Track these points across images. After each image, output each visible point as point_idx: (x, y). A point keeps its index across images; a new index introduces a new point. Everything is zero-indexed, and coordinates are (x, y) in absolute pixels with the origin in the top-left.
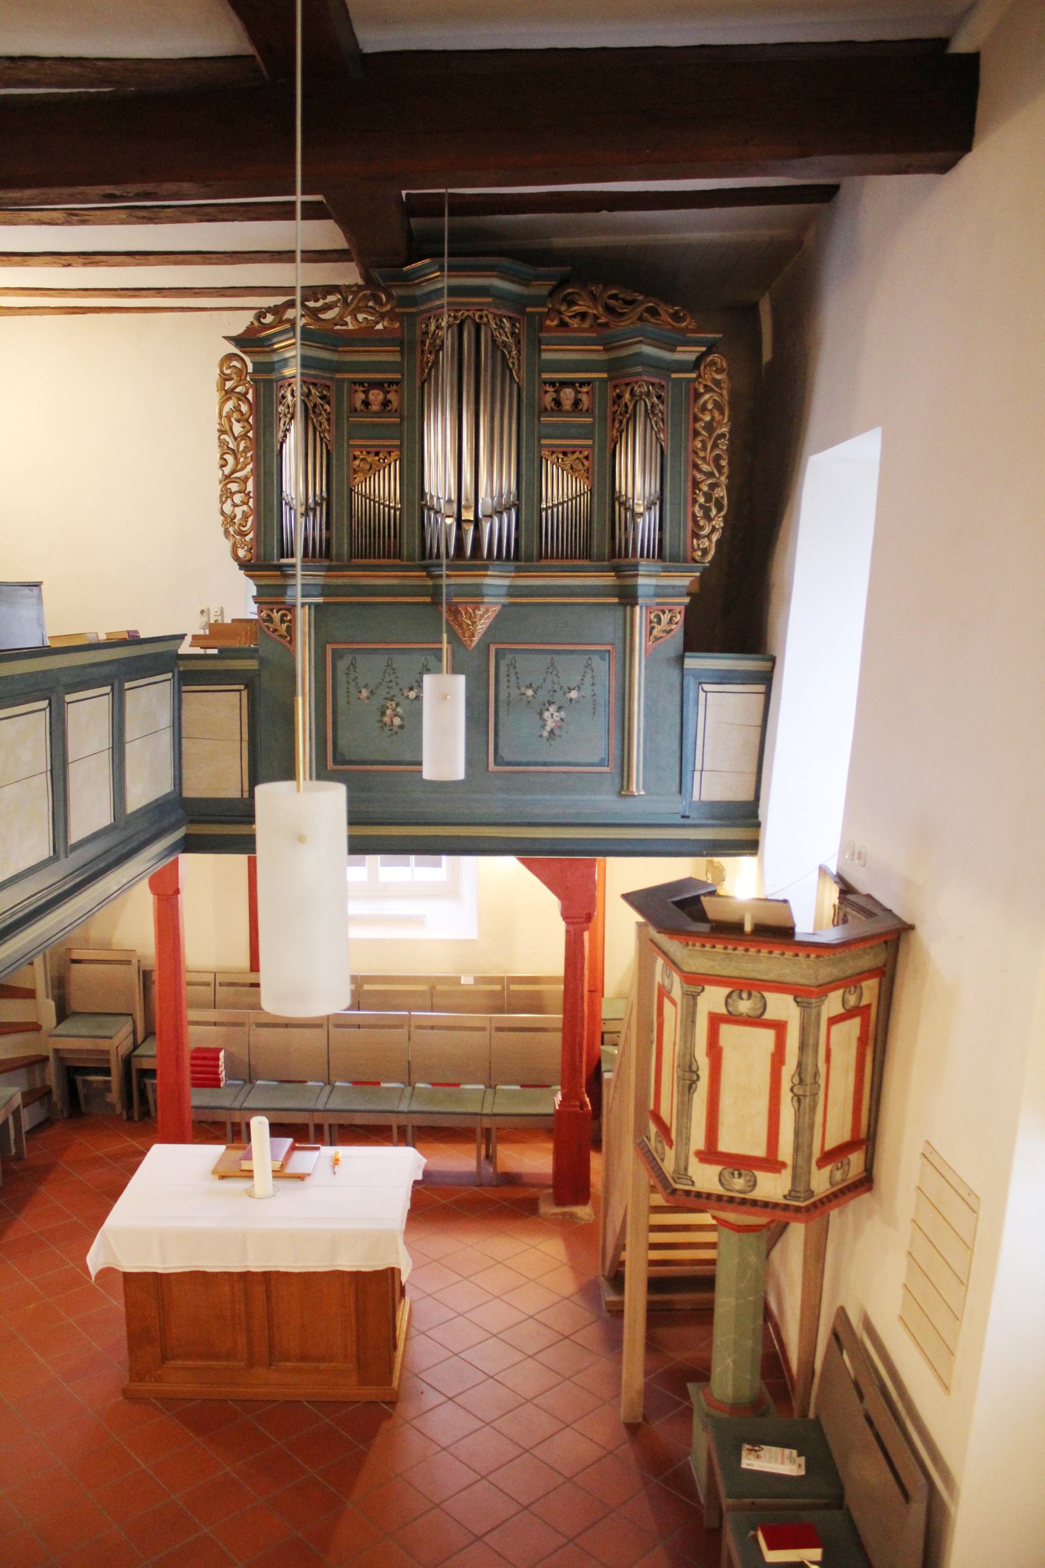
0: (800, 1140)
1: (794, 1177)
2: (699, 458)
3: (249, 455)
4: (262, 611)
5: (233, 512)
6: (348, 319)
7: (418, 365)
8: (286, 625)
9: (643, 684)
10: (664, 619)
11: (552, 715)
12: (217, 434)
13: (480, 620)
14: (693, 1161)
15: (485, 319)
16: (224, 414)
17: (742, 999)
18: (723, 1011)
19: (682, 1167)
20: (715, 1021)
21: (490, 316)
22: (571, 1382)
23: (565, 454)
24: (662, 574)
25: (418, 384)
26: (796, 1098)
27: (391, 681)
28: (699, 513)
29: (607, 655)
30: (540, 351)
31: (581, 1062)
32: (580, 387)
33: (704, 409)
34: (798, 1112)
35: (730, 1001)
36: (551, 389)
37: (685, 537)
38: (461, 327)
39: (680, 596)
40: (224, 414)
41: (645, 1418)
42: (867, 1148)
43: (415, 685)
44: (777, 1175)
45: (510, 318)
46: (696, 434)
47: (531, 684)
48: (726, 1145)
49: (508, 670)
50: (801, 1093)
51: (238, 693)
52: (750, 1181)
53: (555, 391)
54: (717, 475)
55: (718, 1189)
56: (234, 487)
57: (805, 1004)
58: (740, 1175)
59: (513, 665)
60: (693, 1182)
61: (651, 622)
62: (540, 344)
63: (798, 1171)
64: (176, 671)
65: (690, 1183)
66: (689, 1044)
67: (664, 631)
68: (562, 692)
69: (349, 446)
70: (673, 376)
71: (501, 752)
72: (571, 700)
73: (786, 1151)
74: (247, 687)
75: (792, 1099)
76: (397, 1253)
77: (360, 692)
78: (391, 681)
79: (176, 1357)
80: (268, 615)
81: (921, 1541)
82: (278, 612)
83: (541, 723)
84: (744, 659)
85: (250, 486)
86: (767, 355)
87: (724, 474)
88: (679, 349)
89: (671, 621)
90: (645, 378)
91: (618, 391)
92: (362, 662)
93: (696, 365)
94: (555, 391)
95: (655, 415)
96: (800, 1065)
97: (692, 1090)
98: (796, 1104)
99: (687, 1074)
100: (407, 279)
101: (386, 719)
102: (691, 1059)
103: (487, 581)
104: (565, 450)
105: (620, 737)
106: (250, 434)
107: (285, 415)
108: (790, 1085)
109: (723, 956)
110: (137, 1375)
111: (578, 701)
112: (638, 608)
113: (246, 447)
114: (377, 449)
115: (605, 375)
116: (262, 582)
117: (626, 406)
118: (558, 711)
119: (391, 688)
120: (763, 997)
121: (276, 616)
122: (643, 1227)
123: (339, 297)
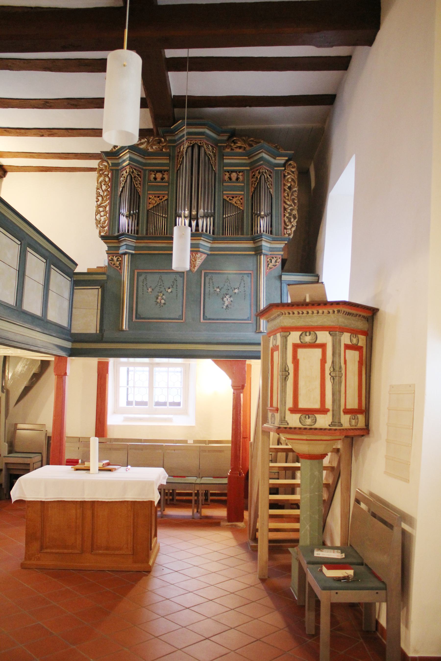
0: (335, 397)
1: (333, 415)
2: (286, 199)
3: (108, 197)
4: (109, 257)
5: (100, 218)
6: (149, 148)
7: (176, 163)
8: (119, 262)
9: (265, 286)
10: (273, 261)
11: (227, 299)
12: (96, 189)
13: (198, 259)
14: (288, 413)
15: (202, 144)
16: (99, 182)
17: (306, 336)
18: (299, 342)
19: (283, 416)
20: (296, 347)
21: (204, 143)
22: (235, 652)
23: (233, 197)
24: (272, 242)
25: (176, 171)
26: (332, 378)
27: (161, 285)
28: (287, 220)
29: (250, 275)
30: (223, 159)
31: (240, 453)
32: (239, 173)
33: (288, 181)
34: (333, 384)
35: (301, 337)
36: (227, 174)
37: (281, 229)
38: (193, 147)
39: (279, 251)
40: (99, 182)
41: (269, 577)
42: (366, 414)
43: (171, 287)
44: (326, 415)
45: (212, 146)
46: (285, 190)
47: (219, 287)
48: (301, 405)
49: (209, 281)
50: (334, 375)
51: (97, 290)
52: (313, 419)
53: (229, 175)
54: (293, 206)
55: (299, 425)
56: (101, 209)
57: (334, 335)
58: (309, 417)
59: (211, 279)
60: (288, 424)
61: (268, 262)
62: (223, 156)
63: (335, 412)
64: (72, 279)
65: (287, 424)
66: (284, 359)
67: (273, 265)
68: (231, 290)
69: (147, 193)
70: (275, 168)
71: (206, 314)
72: (235, 293)
73: (329, 404)
74: (101, 287)
75: (330, 378)
76: (154, 493)
77: (148, 289)
78: (161, 285)
79: (46, 548)
80: (112, 258)
81: (400, 549)
82: (116, 257)
83: (223, 302)
84: (306, 276)
85: (108, 209)
86: (313, 185)
87: (296, 205)
88: (277, 158)
89: (276, 262)
90: (265, 167)
91: (254, 173)
92: (149, 277)
93: (284, 165)
94: (229, 175)
95: (268, 182)
96: (333, 362)
97: (286, 380)
98: (332, 381)
99: (284, 372)
100: (172, 132)
101: (158, 301)
102: (285, 366)
103: (201, 242)
104: (233, 196)
105: (255, 280)
106: (109, 190)
107: (123, 181)
108: (329, 372)
109: (298, 317)
110: (28, 557)
111: (238, 294)
112: (262, 256)
113: (107, 194)
114: (159, 195)
115: (248, 168)
116: (110, 245)
117: (257, 178)
118: (230, 298)
119: (161, 288)
120: (315, 333)
121: (115, 259)
122: (266, 530)
123: (146, 140)
